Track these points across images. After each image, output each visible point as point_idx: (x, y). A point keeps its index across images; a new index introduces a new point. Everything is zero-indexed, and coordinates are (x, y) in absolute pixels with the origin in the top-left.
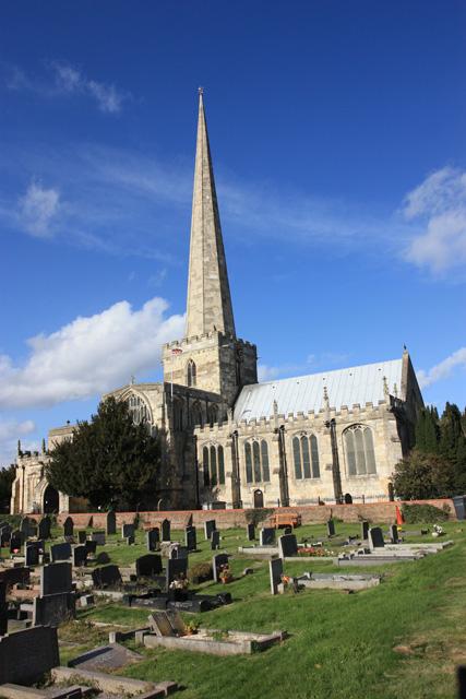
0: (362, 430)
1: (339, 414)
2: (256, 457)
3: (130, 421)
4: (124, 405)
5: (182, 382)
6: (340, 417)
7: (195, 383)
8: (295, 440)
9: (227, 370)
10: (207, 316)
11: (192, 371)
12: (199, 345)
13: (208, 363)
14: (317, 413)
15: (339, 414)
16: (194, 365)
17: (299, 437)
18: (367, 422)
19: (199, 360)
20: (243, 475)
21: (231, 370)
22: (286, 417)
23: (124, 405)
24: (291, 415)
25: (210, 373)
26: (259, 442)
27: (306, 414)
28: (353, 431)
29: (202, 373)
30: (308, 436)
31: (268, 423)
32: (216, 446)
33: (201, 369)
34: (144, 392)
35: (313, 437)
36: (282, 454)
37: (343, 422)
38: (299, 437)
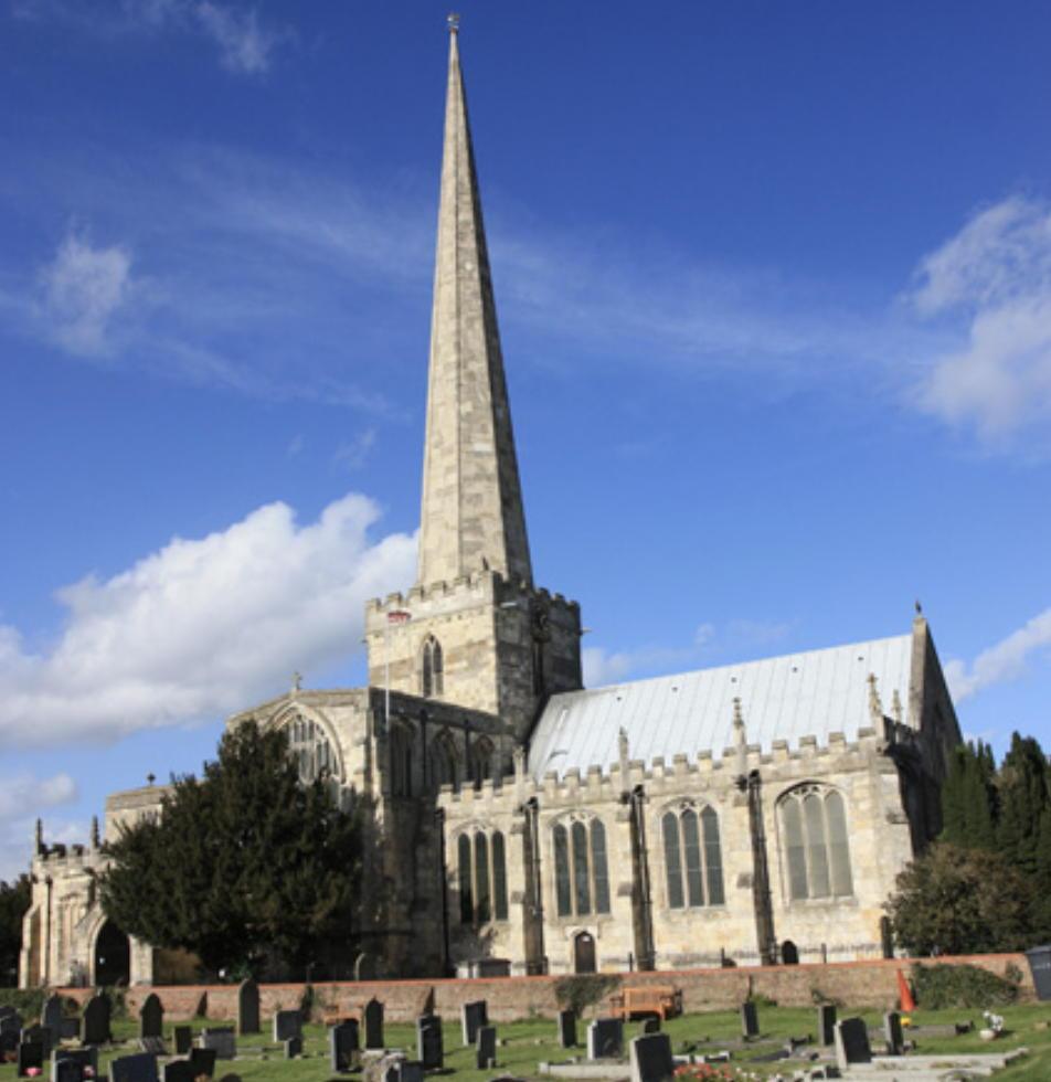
0: (821, 795)
1: (767, 760)
2: (580, 857)
3: (293, 774)
4: (279, 739)
5: (410, 686)
6: (771, 767)
7: (440, 689)
8: (669, 820)
9: (513, 660)
10: (468, 538)
11: (432, 663)
12: (448, 603)
13: (470, 645)
14: (717, 756)
15: (767, 760)
16: (438, 649)
17: (677, 812)
18: (833, 778)
19: (451, 637)
20: (549, 899)
21: (520, 656)
22: (649, 767)
23: (279, 739)
24: (659, 762)
25: (474, 665)
26: (586, 823)
27: (693, 760)
28: (800, 798)
29: (457, 666)
30: (698, 810)
31: (606, 780)
32: (488, 833)
33: (455, 657)
34: (325, 710)
35: (709, 813)
36: (639, 851)
37: (777, 777)
38: (677, 812)
